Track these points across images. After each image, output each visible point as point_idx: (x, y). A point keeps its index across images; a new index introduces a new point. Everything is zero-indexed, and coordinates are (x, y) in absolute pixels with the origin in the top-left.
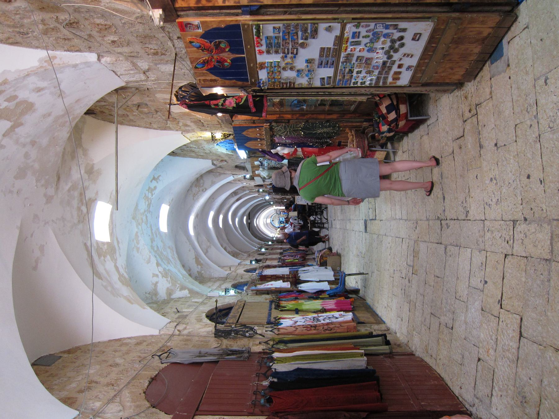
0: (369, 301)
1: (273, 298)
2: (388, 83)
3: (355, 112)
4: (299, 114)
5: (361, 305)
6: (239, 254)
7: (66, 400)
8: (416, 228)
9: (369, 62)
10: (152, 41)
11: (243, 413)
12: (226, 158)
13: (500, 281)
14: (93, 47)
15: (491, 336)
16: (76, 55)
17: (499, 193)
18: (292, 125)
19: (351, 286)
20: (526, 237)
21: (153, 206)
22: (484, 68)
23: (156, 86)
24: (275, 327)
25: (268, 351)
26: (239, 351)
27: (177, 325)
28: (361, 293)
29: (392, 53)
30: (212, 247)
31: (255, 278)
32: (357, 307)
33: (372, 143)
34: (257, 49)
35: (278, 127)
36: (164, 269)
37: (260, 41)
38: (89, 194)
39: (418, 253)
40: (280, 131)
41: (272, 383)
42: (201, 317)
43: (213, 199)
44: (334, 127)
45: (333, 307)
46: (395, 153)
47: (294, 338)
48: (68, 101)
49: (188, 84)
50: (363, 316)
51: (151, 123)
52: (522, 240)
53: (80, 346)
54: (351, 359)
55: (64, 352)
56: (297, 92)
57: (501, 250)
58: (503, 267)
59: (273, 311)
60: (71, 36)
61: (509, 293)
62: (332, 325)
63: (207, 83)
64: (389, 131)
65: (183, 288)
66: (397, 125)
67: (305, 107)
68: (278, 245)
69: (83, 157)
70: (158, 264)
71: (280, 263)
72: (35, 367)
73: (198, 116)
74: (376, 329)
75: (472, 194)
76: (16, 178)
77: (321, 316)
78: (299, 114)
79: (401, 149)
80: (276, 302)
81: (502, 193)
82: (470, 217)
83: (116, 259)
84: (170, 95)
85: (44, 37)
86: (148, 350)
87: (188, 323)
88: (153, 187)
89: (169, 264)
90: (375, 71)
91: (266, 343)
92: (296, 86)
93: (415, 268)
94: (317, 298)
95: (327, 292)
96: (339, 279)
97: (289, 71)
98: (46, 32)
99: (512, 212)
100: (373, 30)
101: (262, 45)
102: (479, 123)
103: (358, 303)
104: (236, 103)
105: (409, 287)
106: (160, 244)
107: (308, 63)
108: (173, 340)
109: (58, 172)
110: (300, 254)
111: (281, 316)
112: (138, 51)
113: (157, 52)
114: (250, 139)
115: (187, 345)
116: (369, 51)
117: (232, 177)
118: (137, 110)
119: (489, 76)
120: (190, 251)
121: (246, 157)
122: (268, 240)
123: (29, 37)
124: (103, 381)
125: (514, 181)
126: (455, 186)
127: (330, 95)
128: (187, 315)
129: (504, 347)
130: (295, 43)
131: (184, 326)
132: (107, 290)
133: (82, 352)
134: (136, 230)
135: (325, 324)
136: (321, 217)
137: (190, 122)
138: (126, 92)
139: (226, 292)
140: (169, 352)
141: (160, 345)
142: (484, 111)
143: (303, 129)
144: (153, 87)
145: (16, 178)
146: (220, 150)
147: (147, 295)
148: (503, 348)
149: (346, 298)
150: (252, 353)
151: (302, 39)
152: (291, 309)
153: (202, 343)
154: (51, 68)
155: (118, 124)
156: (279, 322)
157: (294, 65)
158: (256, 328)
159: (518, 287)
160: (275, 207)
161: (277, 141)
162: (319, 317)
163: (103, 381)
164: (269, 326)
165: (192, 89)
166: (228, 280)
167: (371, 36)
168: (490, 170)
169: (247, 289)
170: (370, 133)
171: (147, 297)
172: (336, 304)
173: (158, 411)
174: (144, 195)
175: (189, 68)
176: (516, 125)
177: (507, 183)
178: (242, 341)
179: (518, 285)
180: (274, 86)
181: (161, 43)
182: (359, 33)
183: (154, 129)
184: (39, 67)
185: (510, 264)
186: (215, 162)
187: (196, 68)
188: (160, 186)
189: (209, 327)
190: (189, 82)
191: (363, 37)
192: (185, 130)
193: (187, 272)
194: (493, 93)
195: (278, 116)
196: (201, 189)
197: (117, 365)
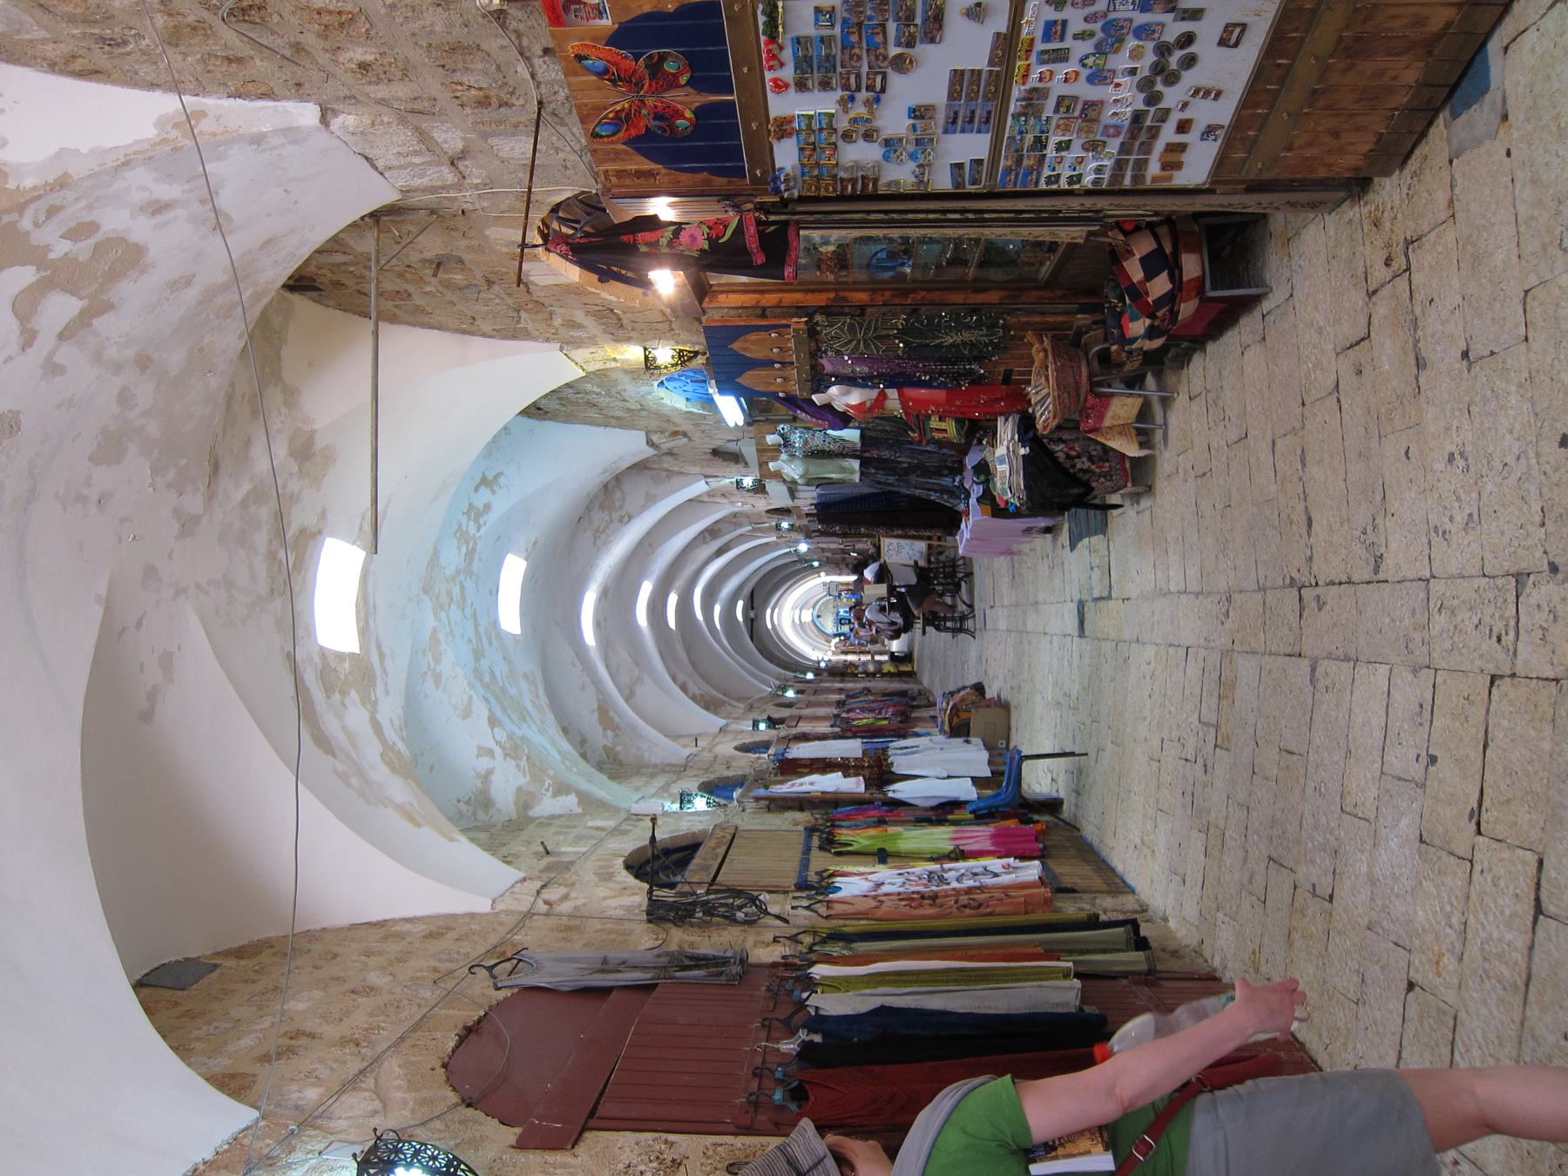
0: (1090, 832)
1: (816, 819)
2: (1148, 181)
3: (1050, 284)
4: (893, 290)
5: (1067, 844)
6: (724, 703)
7: (227, 1080)
8: (1227, 614)
9: (1092, 114)
10: (472, 62)
11: (723, 1128)
12: (686, 426)
13: (1475, 755)
14: (307, 85)
15: (1448, 916)
16: (261, 109)
17: (1474, 495)
18: (871, 321)
19: (1038, 791)
20: (1555, 619)
21: (480, 559)
22: (1432, 130)
23: (485, 204)
24: (820, 898)
25: (797, 961)
26: (715, 958)
27: (543, 887)
28: (1067, 811)
29: (1159, 87)
30: (647, 679)
31: (765, 767)
32: (1054, 847)
33: (1101, 375)
34: (768, 75)
35: (831, 326)
36: (511, 736)
37: (776, 52)
38: (300, 518)
39: (1233, 685)
40: (838, 338)
41: (806, 1046)
42: (612, 867)
43: (650, 545)
44: (992, 327)
45: (987, 845)
46: (1166, 403)
47: (868, 928)
48: (241, 242)
49: (576, 197)
50: (1069, 871)
51: (474, 319)
52: (1543, 629)
53: (270, 938)
54: (1035, 983)
55: (227, 954)
56: (886, 212)
57: (1478, 662)
58: (1484, 713)
59: (815, 853)
60: (244, 50)
61: (1503, 787)
62: (983, 892)
63: (628, 181)
64: (1151, 333)
65: (561, 789)
66: (1174, 314)
67: (908, 270)
68: (834, 681)
69: (284, 410)
70: (493, 722)
71: (837, 729)
72: (145, 991)
73: (605, 295)
74: (1108, 906)
75: (1394, 506)
76: (95, 459)
77: (950, 870)
78: (893, 290)
79: (1186, 389)
80: (822, 832)
81: (1485, 495)
82: (1387, 571)
83: (376, 702)
84: (521, 233)
85: (170, 51)
86: (458, 953)
87: (573, 884)
88: (480, 505)
89: (525, 721)
90: (1110, 141)
91: (793, 939)
92: (882, 190)
93: (1223, 730)
94: (940, 822)
95: (967, 806)
96: (1002, 773)
97: (861, 142)
98: (174, 38)
99: (1512, 549)
100: (1105, 15)
101: (782, 65)
102: (1416, 295)
103: (1055, 838)
104: (709, 239)
105: (1205, 785)
106: (501, 668)
107: (915, 117)
108: (531, 929)
109: (213, 448)
110: (894, 706)
111: (838, 868)
112: (435, 94)
113: (487, 97)
114: (754, 364)
115: (570, 941)
116: (1091, 80)
117: (703, 482)
118: (435, 275)
119: (1446, 155)
120: (583, 688)
121: (741, 423)
122: (805, 670)
123: (129, 54)
124: (331, 1031)
125: (1518, 458)
126: (1342, 484)
127: (980, 220)
128: (572, 863)
129: (1486, 946)
130: (877, 58)
131: (563, 890)
132: (349, 785)
133: (275, 954)
134: (431, 622)
135: (963, 890)
136: (954, 601)
137: (583, 314)
138: (403, 221)
139: (681, 803)
140: (517, 958)
141: (494, 939)
142: (1429, 258)
143: (903, 333)
144: (477, 206)
145: (95, 459)
146: (668, 402)
147: (463, 807)
148: (1483, 950)
149: (1022, 822)
150: (750, 965)
151: (898, 45)
152: (865, 850)
153: (613, 936)
154: (191, 143)
155: (381, 317)
156: (829, 884)
157: (876, 124)
158: (764, 897)
159: (1530, 768)
160: (824, 578)
161: (828, 368)
162: (944, 870)
163: (331, 1031)
164: (804, 894)
165: (588, 214)
166: (689, 772)
167: (1100, 35)
168: (1447, 429)
169: (742, 795)
170: (1096, 343)
171: (460, 812)
172: (996, 837)
173: (480, 1115)
174: (455, 527)
175: (577, 147)
176: (1526, 292)
177: (1497, 464)
178: (725, 933)
179: (1531, 762)
180: (818, 189)
181: (498, 67)
182: (1064, 23)
183: (484, 335)
184: (158, 140)
185: (1505, 701)
186: (655, 438)
187: (595, 135)
188: (502, 502)
189: (633, 895)
190: (577, 190)
191: (1076, 37)
192: (569, 341)
193: (577, 750)
194: (1456, 203)
195: (832, 295)
196: (616, 516)
197: (371, 990)
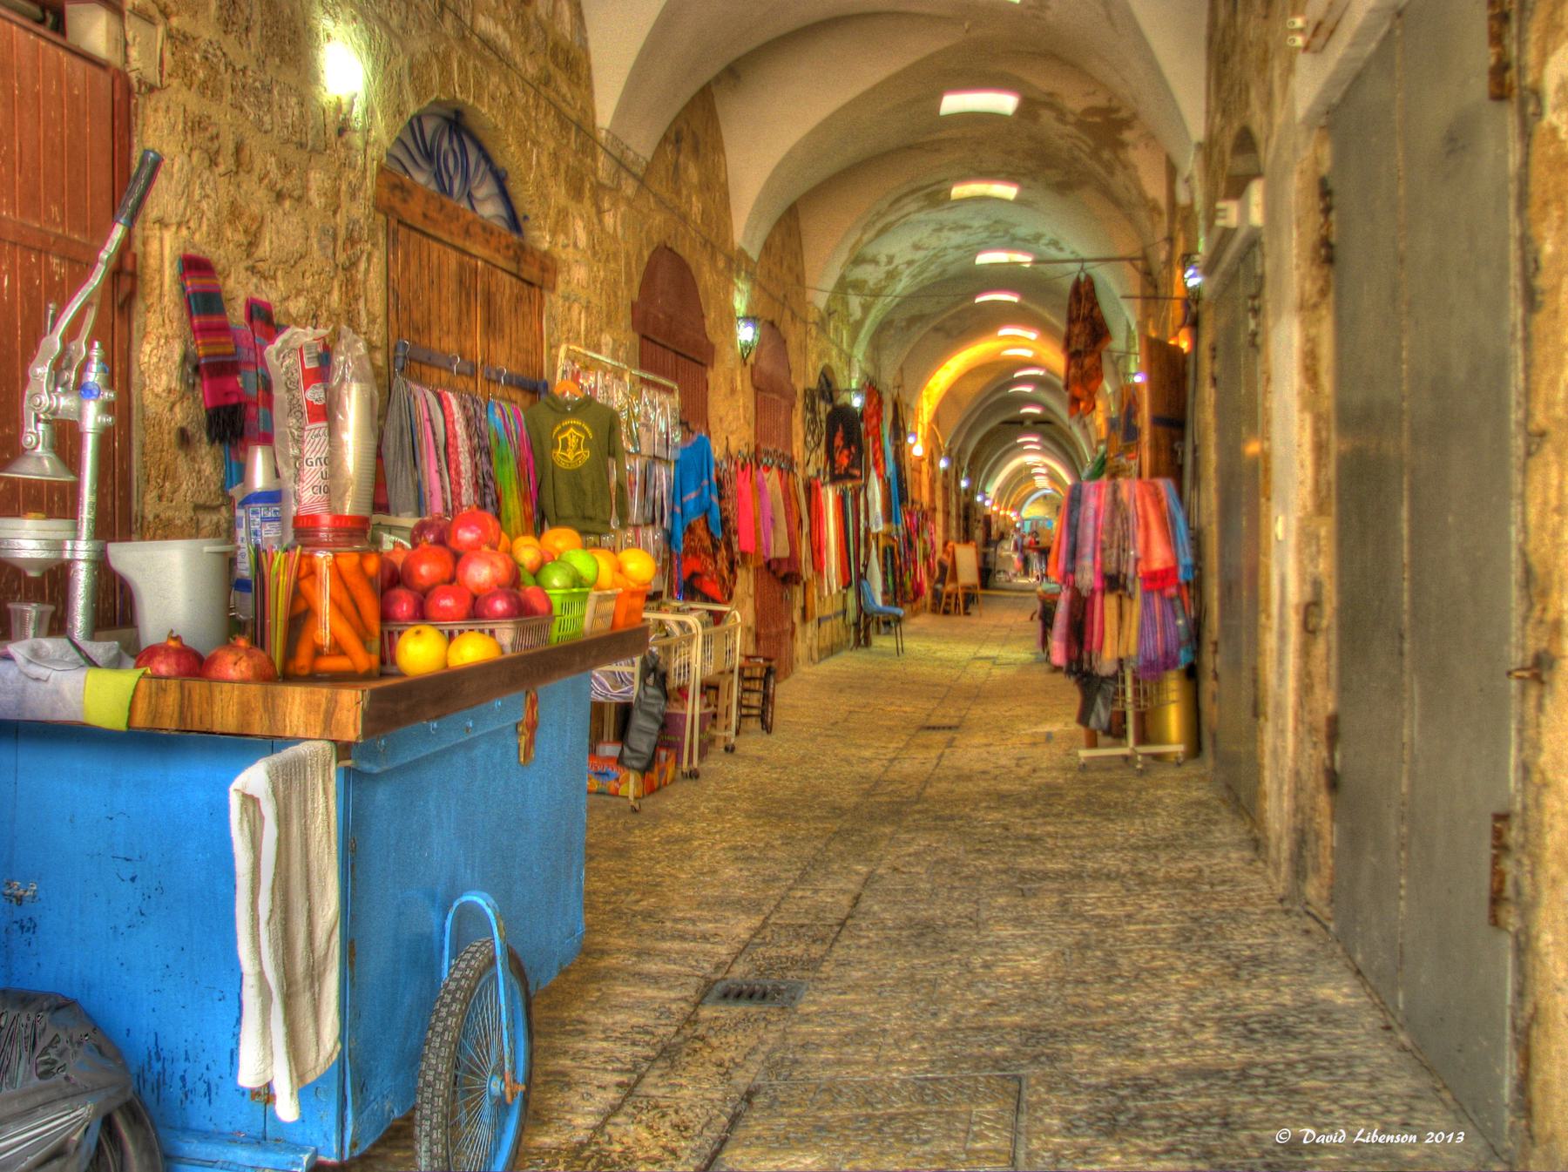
65: (866, 309)
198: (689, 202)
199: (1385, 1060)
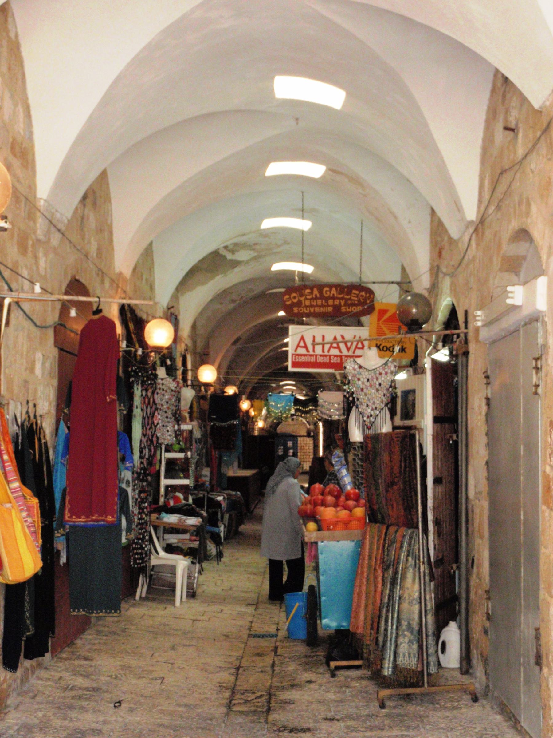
198: (89, 243)
199: (22, 133)
